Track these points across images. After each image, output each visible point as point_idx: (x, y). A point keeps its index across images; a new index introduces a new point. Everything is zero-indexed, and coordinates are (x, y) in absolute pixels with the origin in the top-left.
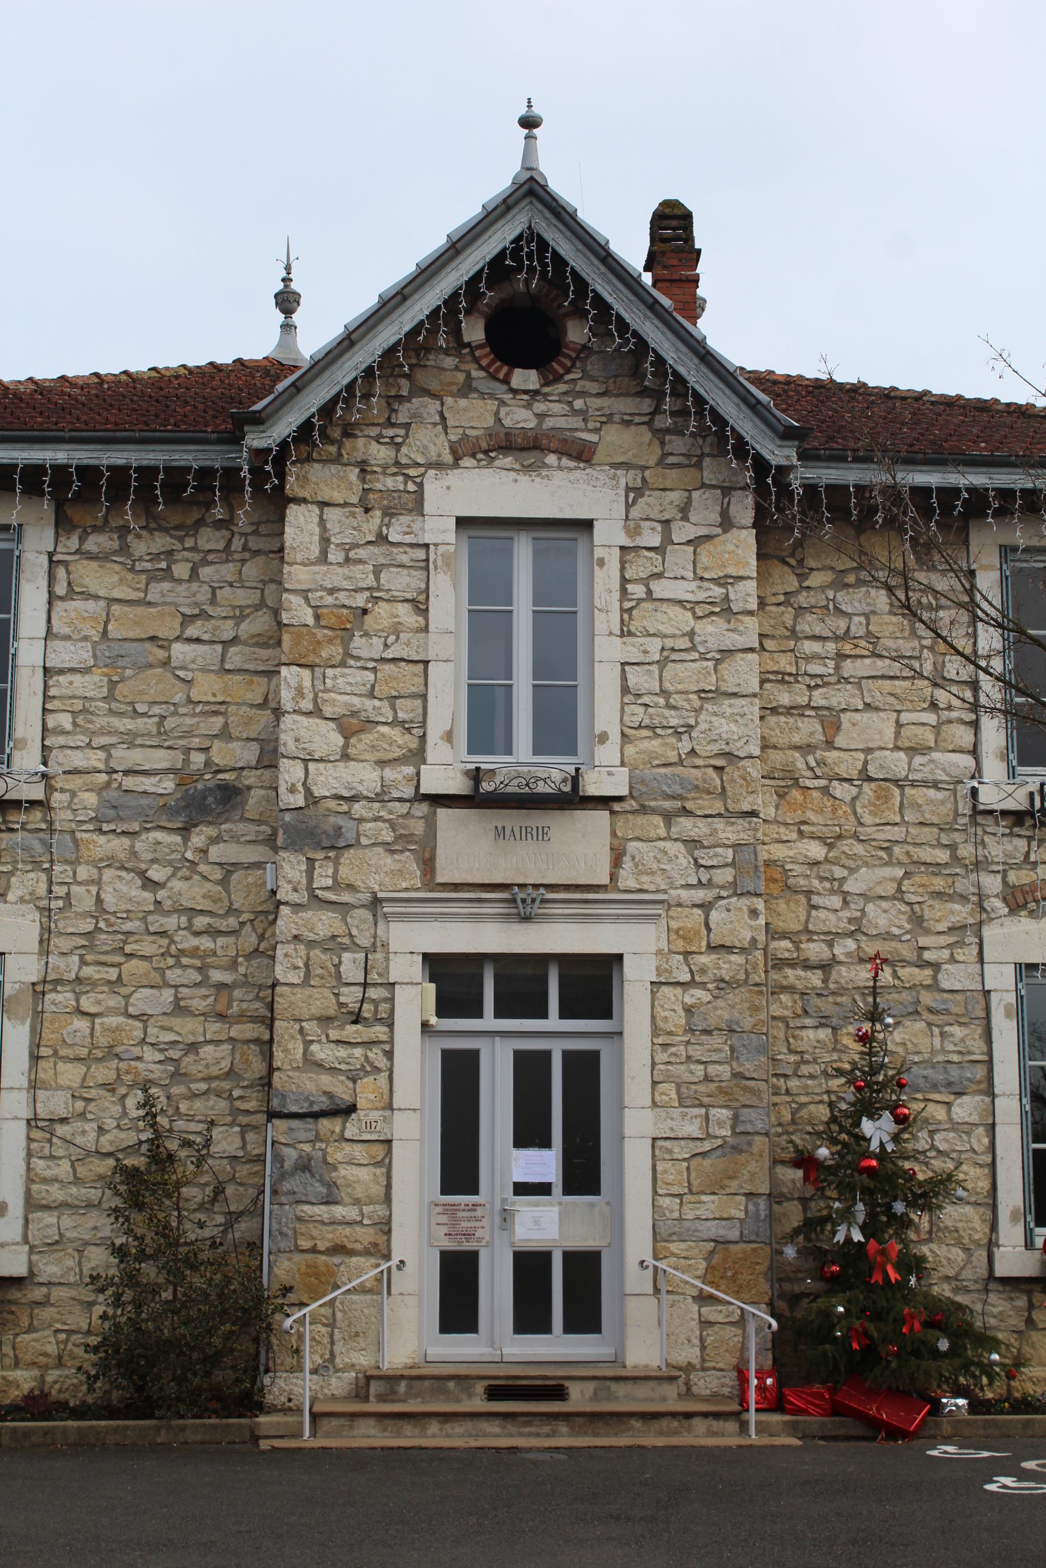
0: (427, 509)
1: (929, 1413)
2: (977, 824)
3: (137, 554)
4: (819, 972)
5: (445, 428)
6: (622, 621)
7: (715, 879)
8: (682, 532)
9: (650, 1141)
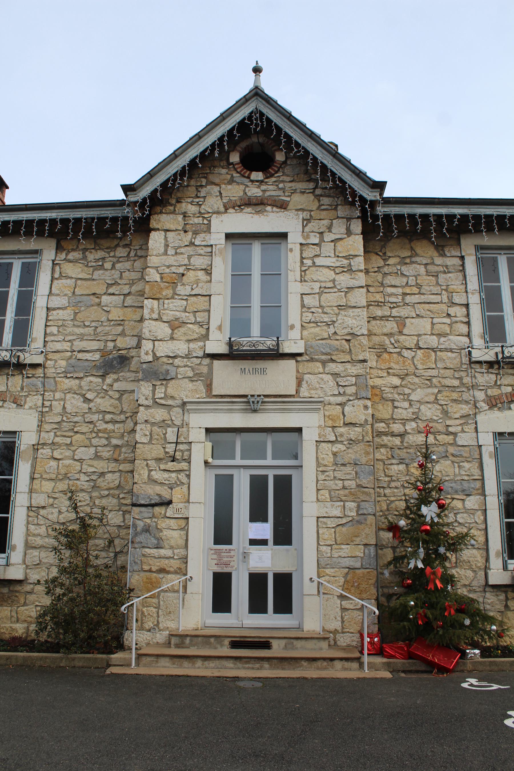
0: (212, 230)
1: (460, 658)
2: (471, 368)
3: (89, 259)
4: (399, 438)
5: (221, 197)
6: (301, 275)
7: (347, 392)
8: (328, 237)
9: (316, 519)
